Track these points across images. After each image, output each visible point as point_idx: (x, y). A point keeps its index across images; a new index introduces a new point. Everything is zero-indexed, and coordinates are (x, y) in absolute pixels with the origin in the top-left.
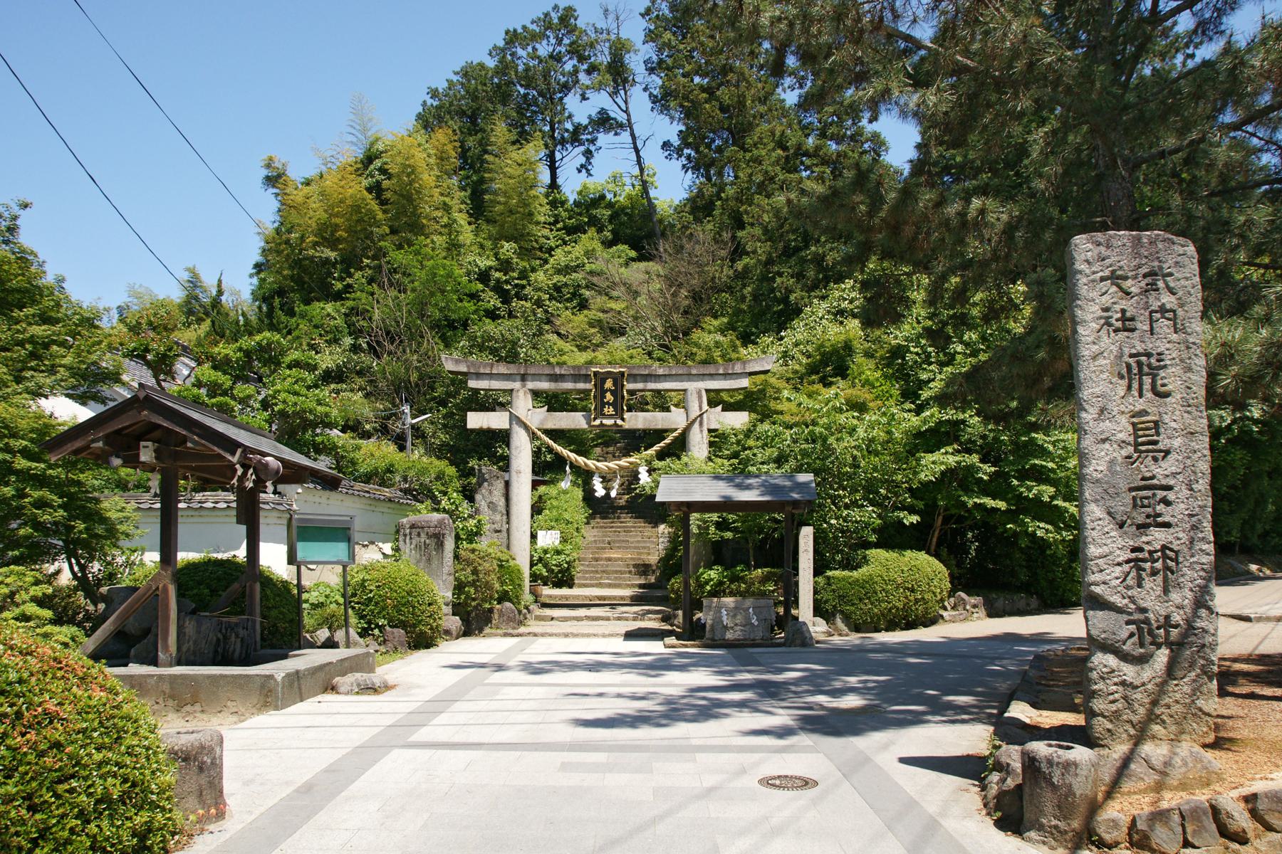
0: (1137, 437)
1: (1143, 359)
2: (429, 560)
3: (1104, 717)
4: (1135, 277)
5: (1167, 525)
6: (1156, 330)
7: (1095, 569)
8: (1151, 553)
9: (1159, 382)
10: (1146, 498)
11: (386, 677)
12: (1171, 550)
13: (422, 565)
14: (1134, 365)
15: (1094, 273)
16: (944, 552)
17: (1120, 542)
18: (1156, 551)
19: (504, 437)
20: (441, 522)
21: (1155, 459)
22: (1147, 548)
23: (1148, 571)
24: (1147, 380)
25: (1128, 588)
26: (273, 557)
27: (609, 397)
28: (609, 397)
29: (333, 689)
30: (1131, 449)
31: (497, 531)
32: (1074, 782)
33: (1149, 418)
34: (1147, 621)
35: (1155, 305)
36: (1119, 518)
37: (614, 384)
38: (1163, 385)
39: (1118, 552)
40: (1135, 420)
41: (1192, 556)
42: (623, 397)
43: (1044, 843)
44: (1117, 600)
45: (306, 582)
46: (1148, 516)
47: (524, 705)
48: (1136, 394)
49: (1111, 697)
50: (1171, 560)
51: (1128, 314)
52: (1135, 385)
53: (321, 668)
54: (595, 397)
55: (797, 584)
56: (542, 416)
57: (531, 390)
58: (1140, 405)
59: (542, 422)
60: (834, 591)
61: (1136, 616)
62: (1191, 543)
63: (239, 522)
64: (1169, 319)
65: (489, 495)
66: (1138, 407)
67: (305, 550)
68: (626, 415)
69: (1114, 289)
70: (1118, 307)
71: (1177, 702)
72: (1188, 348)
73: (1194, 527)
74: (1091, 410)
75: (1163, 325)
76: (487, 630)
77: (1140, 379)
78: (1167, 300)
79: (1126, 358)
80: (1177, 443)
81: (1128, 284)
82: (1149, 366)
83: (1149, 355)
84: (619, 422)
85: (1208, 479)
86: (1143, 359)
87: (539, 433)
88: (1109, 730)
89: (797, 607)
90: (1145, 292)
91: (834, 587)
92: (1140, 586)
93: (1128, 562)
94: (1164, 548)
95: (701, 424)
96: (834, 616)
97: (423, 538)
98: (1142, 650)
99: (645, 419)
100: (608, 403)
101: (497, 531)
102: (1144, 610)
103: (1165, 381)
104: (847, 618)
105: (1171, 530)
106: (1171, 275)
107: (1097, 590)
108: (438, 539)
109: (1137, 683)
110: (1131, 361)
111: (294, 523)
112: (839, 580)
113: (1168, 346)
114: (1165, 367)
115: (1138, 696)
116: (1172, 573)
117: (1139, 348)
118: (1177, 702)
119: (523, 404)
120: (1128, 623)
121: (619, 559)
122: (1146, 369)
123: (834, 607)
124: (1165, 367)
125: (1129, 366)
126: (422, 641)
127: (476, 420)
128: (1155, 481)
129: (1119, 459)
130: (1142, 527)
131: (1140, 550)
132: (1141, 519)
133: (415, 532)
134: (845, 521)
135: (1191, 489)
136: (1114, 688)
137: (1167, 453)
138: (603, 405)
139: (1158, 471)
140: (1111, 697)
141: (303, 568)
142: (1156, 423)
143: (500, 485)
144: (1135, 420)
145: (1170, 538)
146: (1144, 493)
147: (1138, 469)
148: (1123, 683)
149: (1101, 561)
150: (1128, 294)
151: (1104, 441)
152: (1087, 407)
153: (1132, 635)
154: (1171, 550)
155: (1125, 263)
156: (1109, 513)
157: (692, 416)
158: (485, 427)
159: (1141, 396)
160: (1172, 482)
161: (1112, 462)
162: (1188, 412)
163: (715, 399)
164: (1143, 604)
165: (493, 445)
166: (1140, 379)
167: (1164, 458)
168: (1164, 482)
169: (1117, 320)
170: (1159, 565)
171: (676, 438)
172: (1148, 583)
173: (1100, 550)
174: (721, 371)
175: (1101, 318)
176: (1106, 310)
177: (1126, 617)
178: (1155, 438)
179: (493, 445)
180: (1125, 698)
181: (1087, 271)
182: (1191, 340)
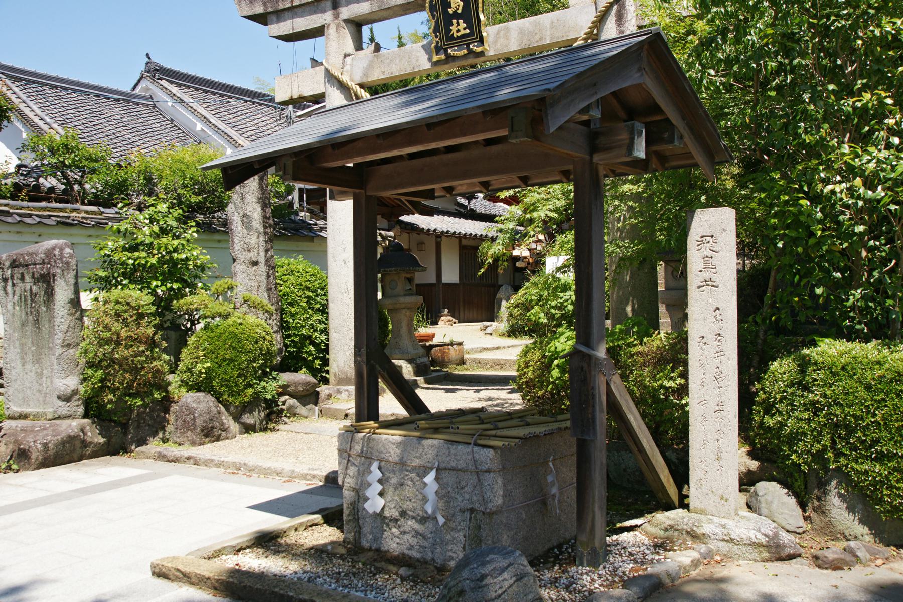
16: (641, 80)
31: (255, 264)
57: (347, 21)
60: (814, 408)
76: (154, 446)
91: (814, 396)
96: (822, 485)
99: (521, 31)
100: (456, 15)
101: (255, 264)
104: (864, 499)
108: (46, 280)
112: (836, 372)
123: (819, 456)
133: (17, 272)
134: (870, 184)
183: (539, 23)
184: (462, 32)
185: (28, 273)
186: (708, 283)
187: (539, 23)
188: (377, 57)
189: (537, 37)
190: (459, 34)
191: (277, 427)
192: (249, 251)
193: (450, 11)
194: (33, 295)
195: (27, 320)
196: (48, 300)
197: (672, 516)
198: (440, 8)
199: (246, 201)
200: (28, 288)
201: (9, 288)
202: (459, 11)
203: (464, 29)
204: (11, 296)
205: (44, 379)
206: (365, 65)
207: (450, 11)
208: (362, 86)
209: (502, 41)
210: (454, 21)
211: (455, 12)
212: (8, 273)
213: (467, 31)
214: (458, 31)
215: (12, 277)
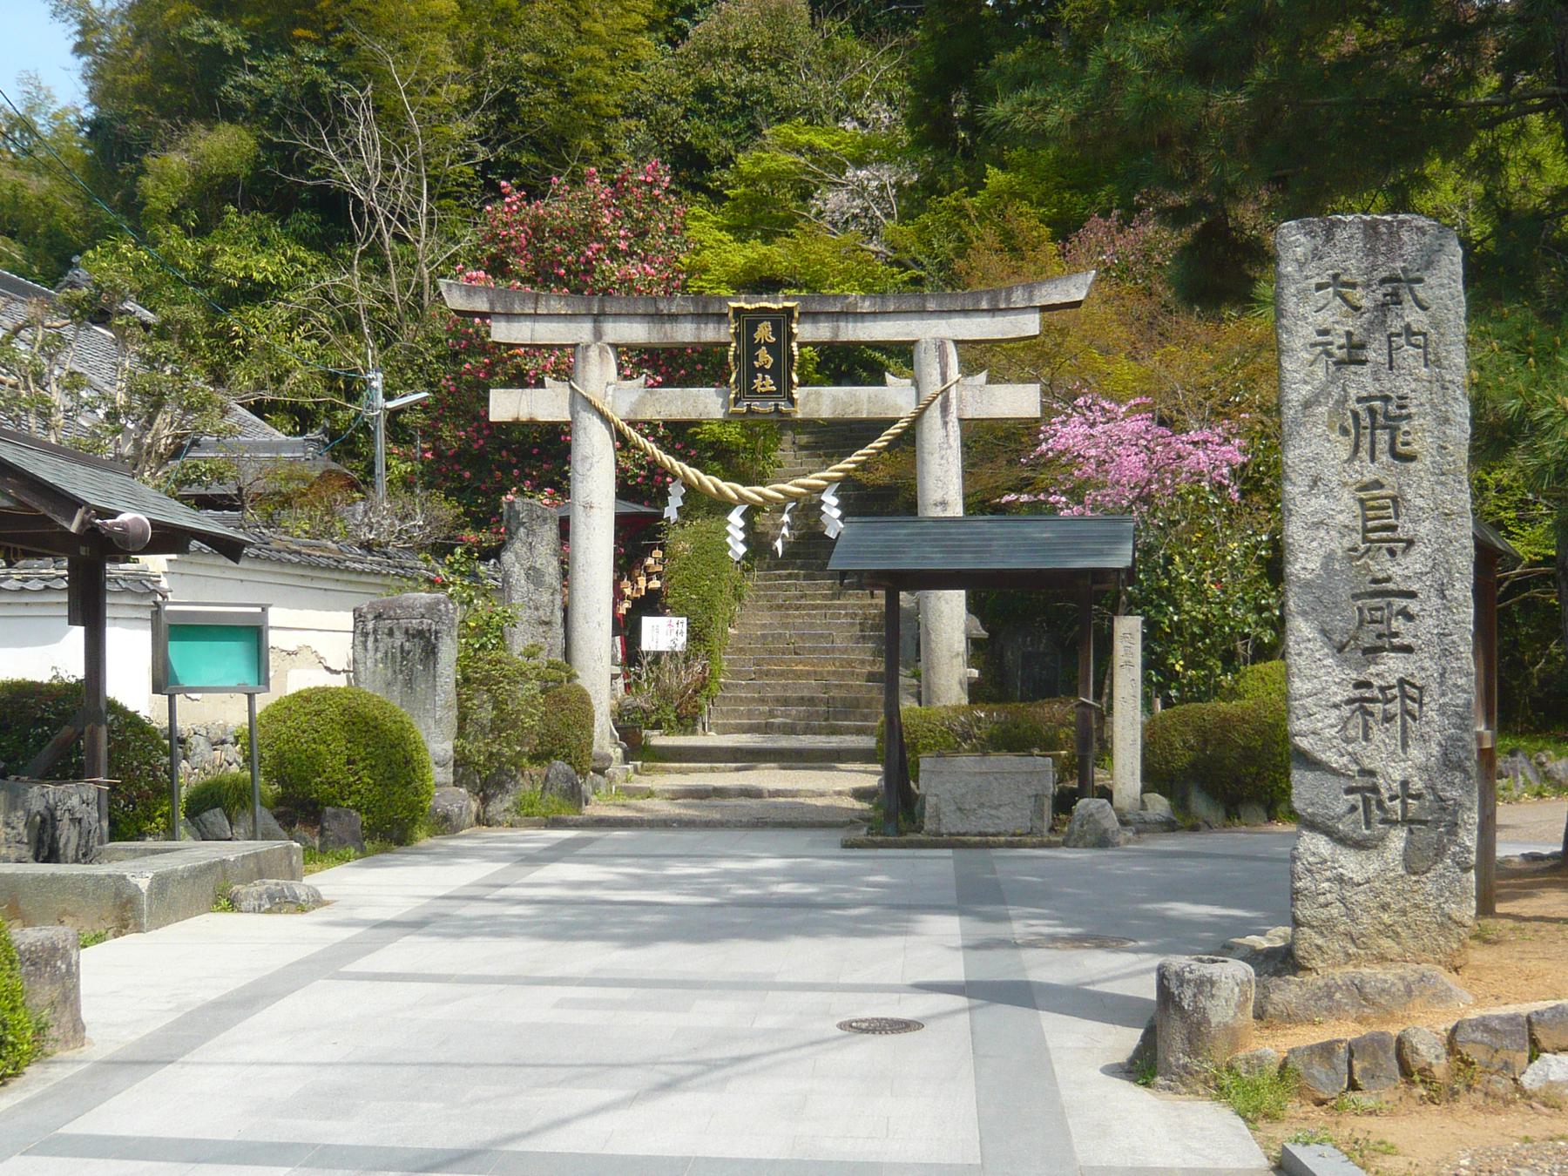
0: (1366, 519)
1: (1377, 404)
2: (409, 683)
3: (1312, 927)
4: (1367, 285)
5: (1408, 649)
6: (1398, 361)
7: (1301, 713)
8: (1382, 689)
9: (1400, 439)
10: (1377, 609)
11: (319, 889)
12: (1413, 686)
13: (396, 689)
14: (1363, 414)
15: (1307, 278)
17: (1338, 674)
18: (1390, 687)
20: (432, 608)
21: (1392, 553)
22: (1377, 682)
23: (1379, 716)
24: (1383, 437)
25: (1348, 741)
26: (129, 682)
27: (764, 358)
28: (764, 358)
29: (233, 905)
30: (1358, 537)
32: (1208, 1005)
33: (1383, 492)
34: (1375, 789)
35: (1397, 326)
36: (1337, 637)
37: (776, 331)
38: (1407, 444)
39: (1334, 688)
40: (1362, 495)
41: (1443, 694)
42: (791, 356)
43: (1170, 1088)
44: (1333, 759)
45: (183, 725)
46: (1380, 636)
48: (1367, 458)
49: (1322, 899)
50: (1413, 700)
51: (1355, 339)
52: (1365, 443)
53: (210, 867)
54: (736, 357)
56: (634, 397)
58: (1371, 472)
61: (1359, 781)
62: (1442, 675)
63: (72, 622)
64: (1418, 347)
65: (529, 553)
66: (1368, 478)
67: (188, 658)
68: (797, 393)
69: (1338, 301)
70: (1341, 329)
71: (1417, 906)
72: (1443, 387)
73: (1445, 653)
74: (1298, 480)
75: (1409, 354)
77: (1373, 434)
78: (1415, 318)
79: (1352, 404)
80: (1424, 529)
81: (1357, 295)
82: (1386, 416)
83: (1386, 399)
84: (783, 406)
85: (1469, 582)
86: (1377, 404)
87: (628, 430)
88: (1319, 947)
89: (1109, 768)
90: (1383, 307)
92: (1366, 738)
93: (1350, 702)
94: (1402, 682)
95: (945, 409)
97: (399, 638)
98: (1367, 832)
100: (762, 369)
102: (1372, 773)
103: (1409, 438)
105: (1413, 657)
106: (1420, 281)
107: (1304, 743)
109: (1357, 878)
110: (1358, 407)
111: (164, 620)
113: (1413, 385)
114: (1409, 417)
115: (1361, 898)
116: (1414, 718)
117: (1372, 389)
118: (1417, 906)
119: (600, 376)
120: (1350, 791)
121: (808, 674)
122: (1380, 420)
124: (1409, 417)
125: (1355, 415)
127: (505, 405)
128: (1391, 586)
129: (1340, 553)
130: (1372, 652)
131: (1368, 685)
132: (1368, 640)
135: (1444, 597)
136: (1326, 885)
137: (1410, 543)
138: (752, 372)
139: (1394, 570)
140: (1322, 899)
141: (178, 698)
142: (1394, 499)
143: (550, 533)
144: (1362, 495)
145: (1411, 668)
146: (1376, 602)
147: (1366, 567)
148: (1340, 879)
149: (1309, 702)
150: (1357, 309)
151: (1318, 525)
152: (1293, 476)
153: (1353, 809)
154: (1413, 686)
155: (1354, 267)
156: (1323, 632)
158: (524, 418)
159: (1373, 460)
160: (1415, 587)
161: (1329, 557)
162: (1443, 484)
163: (976, 356)
164: (1368, 764)
165: (545, 454)
166: (1373, 434)
167: (1405, 551)
168: (1403, 587)
169: (1340, 347)
170: (1395, 707)
171: (898, 437)
172: (1377, 734)
173: (1309, 686)
174: (984, 305)
175: (1313, 345)
176: (1325, 332)
177: (1344, 783)
178: (1392, 521)
179: (545, 454)
180: (1342, 900)
181: (1297, 276)
182: (1448, 377)
185: (399, 628)
186: (1128, 663)
189: (853, 409)
192: (537, 609)
196: (427, 657)
199: (536, 553)
201: (370, 644)
204: (371, 653)
208: (631, 423)
209: (812, 405)
212: (370, 626)
215: (375, 631)
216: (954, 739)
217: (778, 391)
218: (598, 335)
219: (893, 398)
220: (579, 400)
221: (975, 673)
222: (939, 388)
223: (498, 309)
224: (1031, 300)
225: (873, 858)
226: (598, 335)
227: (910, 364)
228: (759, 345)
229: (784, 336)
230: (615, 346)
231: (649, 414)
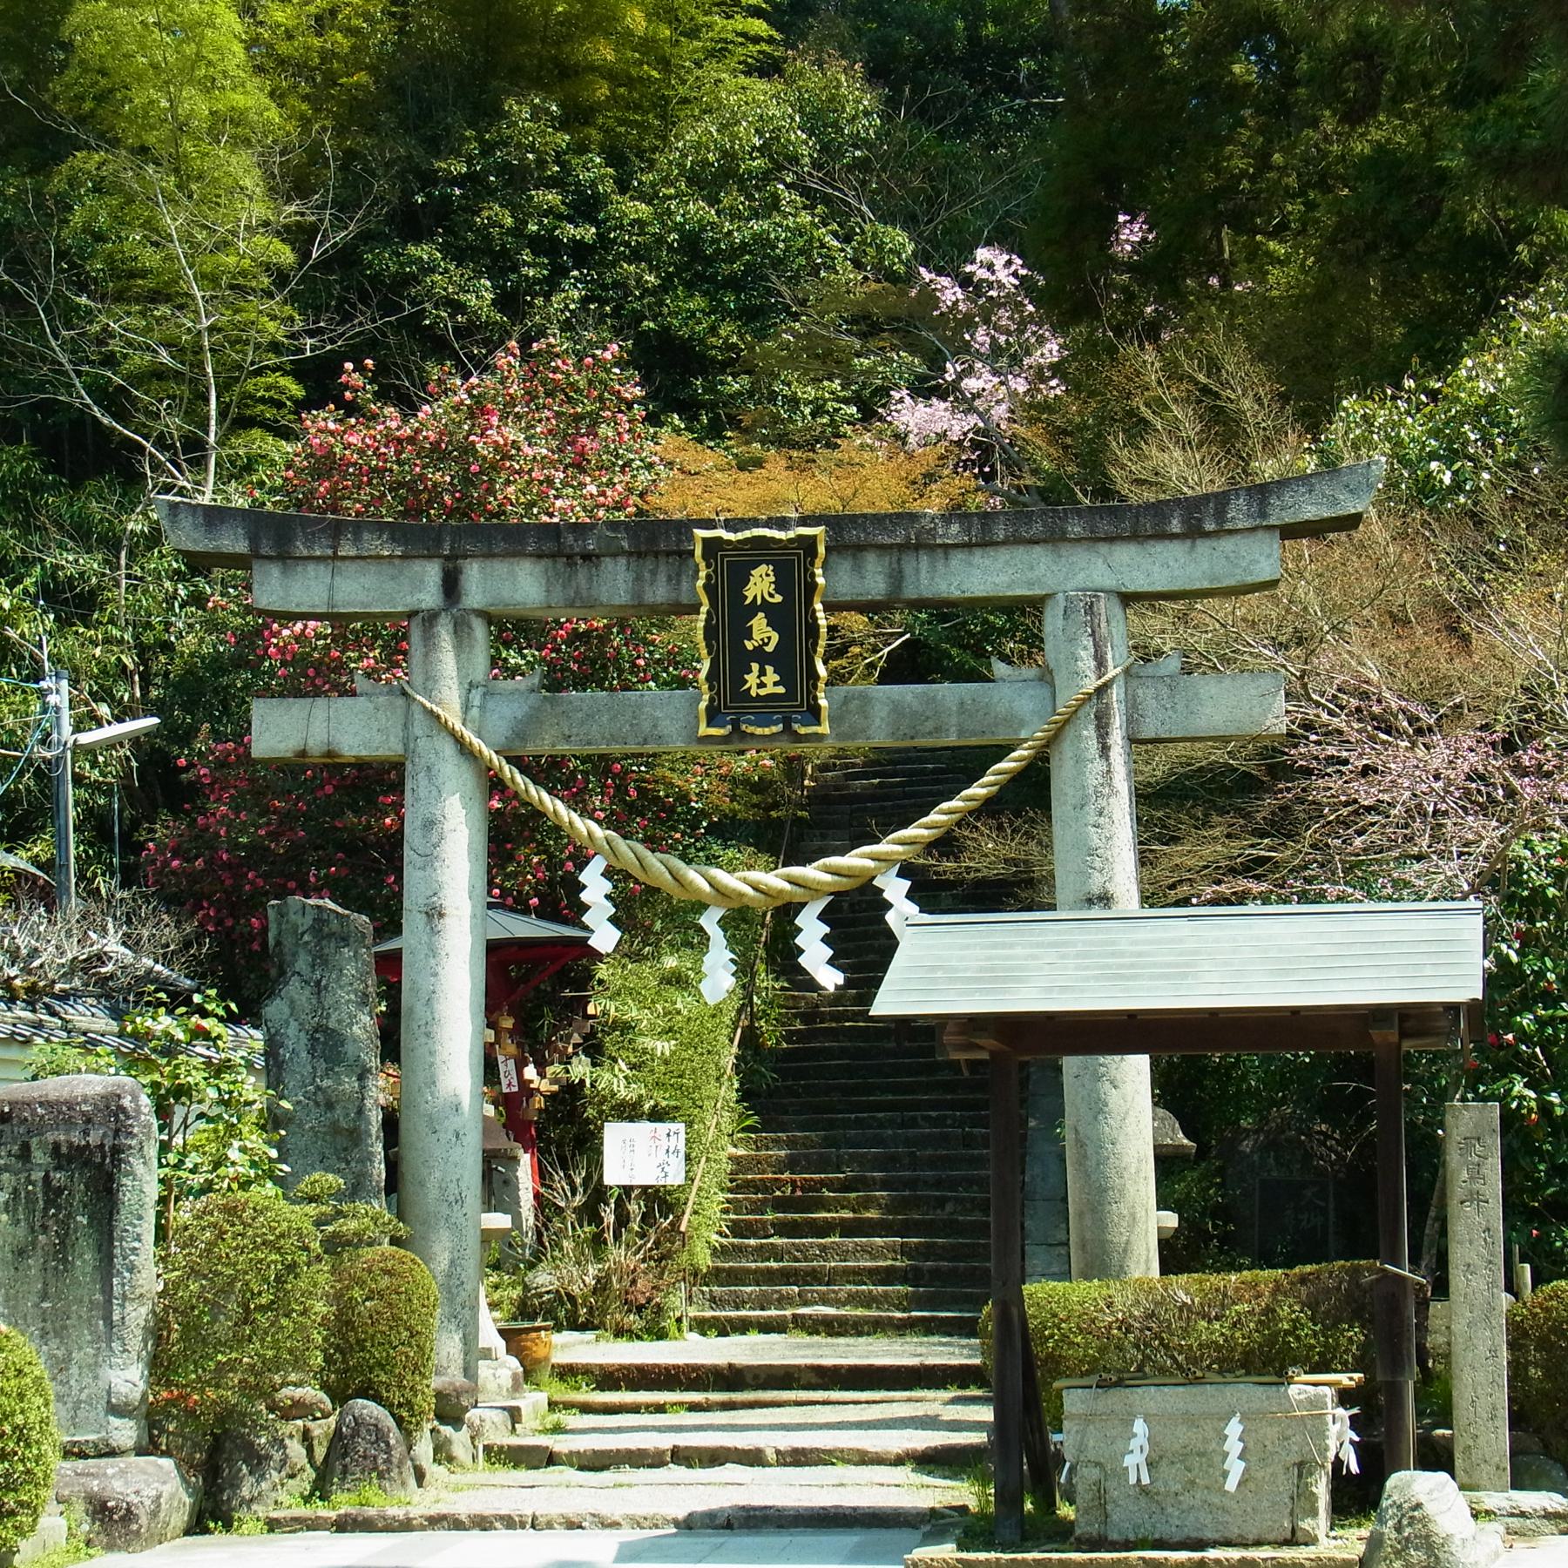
2: (62, 1252)
19: (380, 783)
27: (761, 630)
28: (761, 630)
42: (813, 630)
47: (1424, 948)
55: (1538, 1489)
59: (521, 732)
87: (508, 770)
100: (759, 655)
119: (450, 677)
126: (645, 1188)
127: (279, 729)
143: (353, 969)
157: (1067, 698)
183: (934, 698)
184: (770, 689)
186: (1476, 1198)
187: (934, 698)
188: (553, 702)
190: (763, 692)
191: (34, 1263)
193: (749, 645)
194: (53, 1193)
195: (34, 1243)
197: (909, 698)
198: (724, 636)
200: (38, 1175)
202: (769, 649)
203: (775, 684)
205: (74, 1370)
206: (519, 715)
207: (749, 645)
210: (755, 667)
211: (759, 650)
213: (781, 690)
214: (762, 685)
216: (1143, 1356)
217: (790, 695)
218: (451, 586)
219: (1007, 701)
220: (418, 715)
221: (1171, 1220)
222: (1091, 684)
223: (265, 550)
224: (1263, 515)
225: (909, 1400)
226: (451, 586)
227: (1034, 641)
228: (753, 609)
229: (799, 593)
230: (488, 617)
231: (545, 744)
